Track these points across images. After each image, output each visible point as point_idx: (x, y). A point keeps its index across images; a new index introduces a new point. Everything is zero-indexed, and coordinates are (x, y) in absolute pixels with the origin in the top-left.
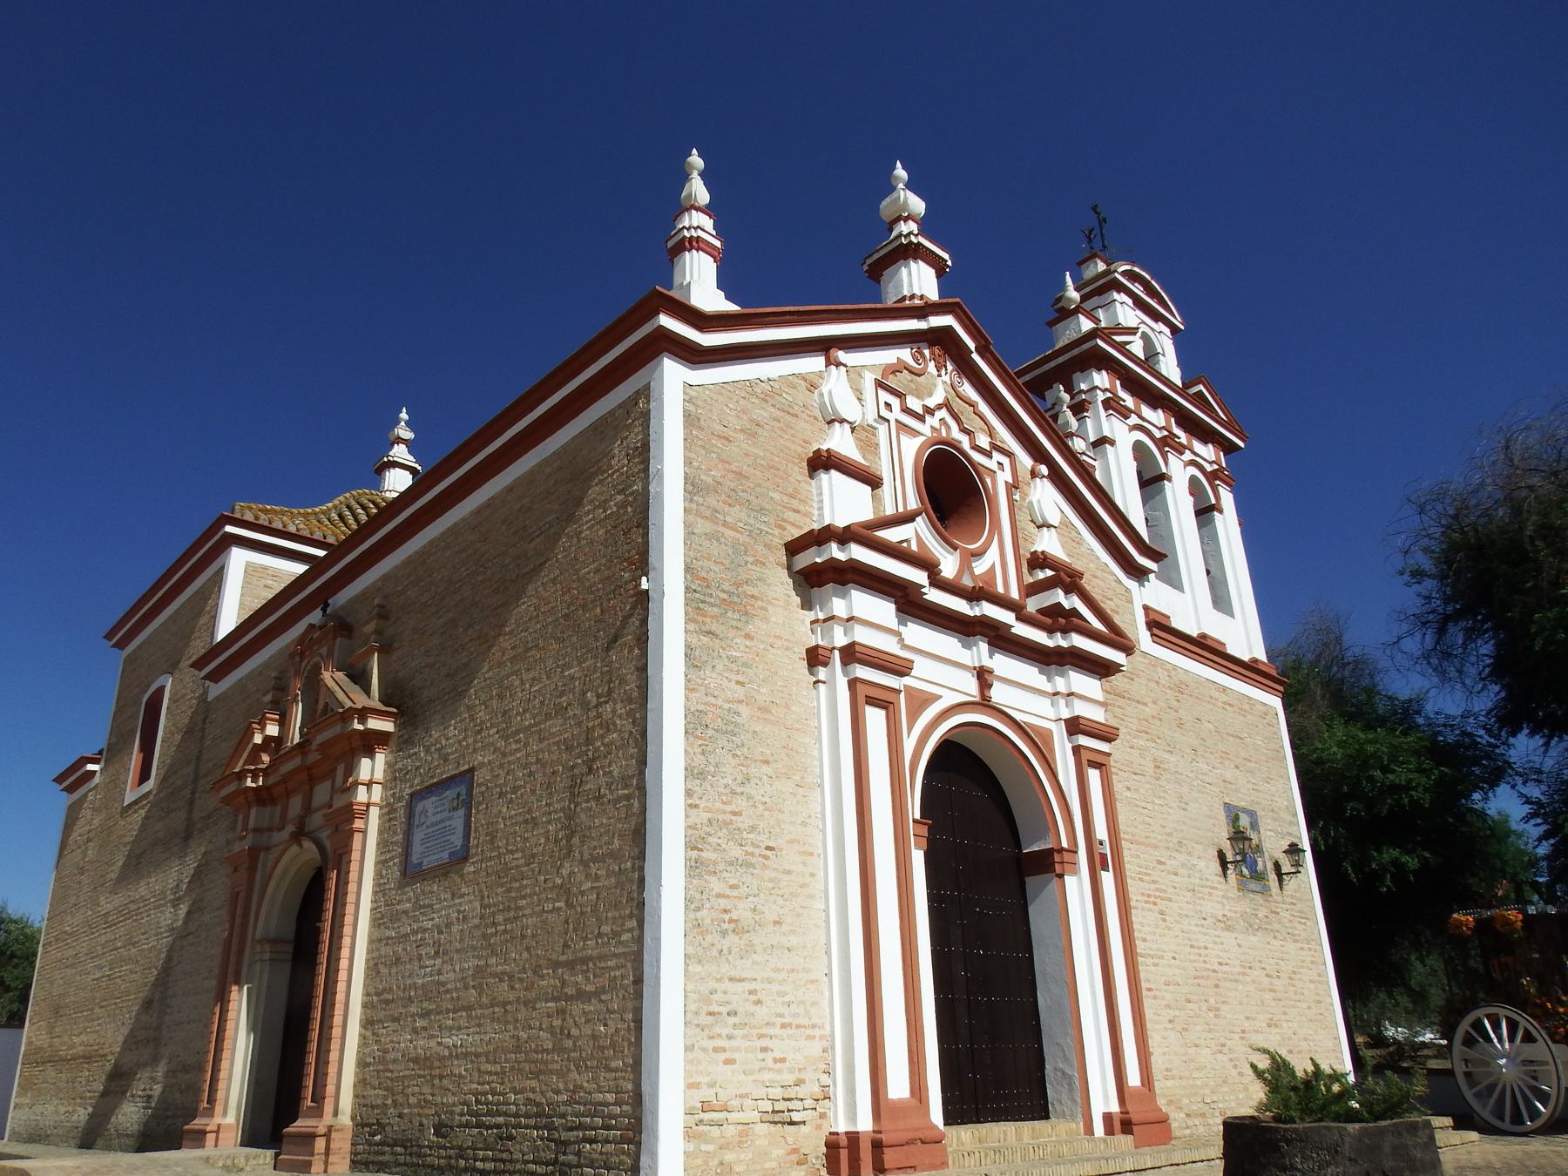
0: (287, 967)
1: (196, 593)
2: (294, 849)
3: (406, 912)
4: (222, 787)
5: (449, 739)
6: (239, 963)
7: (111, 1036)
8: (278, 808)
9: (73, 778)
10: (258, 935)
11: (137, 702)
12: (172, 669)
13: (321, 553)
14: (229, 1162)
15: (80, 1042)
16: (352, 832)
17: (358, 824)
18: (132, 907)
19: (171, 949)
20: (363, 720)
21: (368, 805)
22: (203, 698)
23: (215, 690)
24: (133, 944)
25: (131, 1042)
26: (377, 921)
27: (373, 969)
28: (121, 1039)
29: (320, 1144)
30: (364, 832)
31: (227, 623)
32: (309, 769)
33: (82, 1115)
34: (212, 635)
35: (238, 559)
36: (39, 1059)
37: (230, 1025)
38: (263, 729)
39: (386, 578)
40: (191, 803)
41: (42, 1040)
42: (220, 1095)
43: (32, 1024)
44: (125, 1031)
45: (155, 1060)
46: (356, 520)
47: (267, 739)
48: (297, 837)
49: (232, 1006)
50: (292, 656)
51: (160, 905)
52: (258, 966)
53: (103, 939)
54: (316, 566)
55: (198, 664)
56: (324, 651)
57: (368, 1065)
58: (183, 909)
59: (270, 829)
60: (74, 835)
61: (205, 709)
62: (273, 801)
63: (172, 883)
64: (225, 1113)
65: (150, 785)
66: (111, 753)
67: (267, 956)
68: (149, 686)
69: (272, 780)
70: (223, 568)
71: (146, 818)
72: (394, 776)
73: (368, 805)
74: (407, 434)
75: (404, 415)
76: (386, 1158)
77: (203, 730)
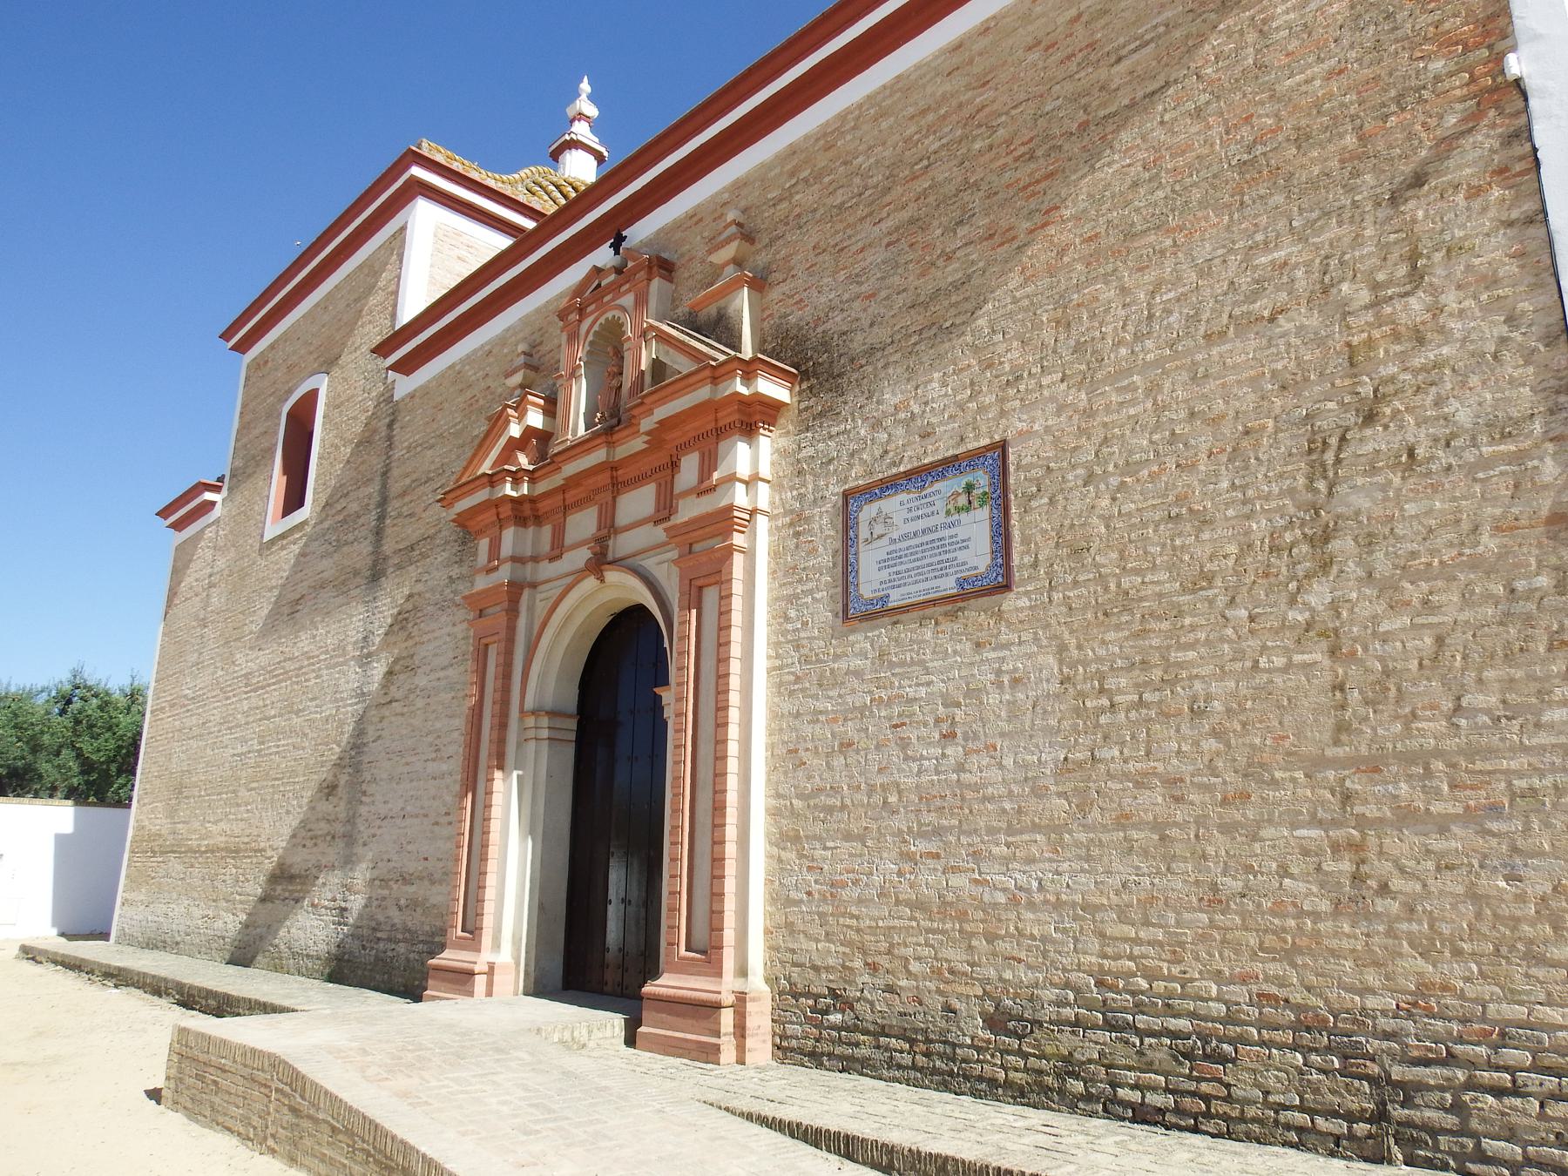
0: (570, 751)
1: (360, 267)
2: (590, 583)
3: (858, 674)
4: (457, 499)
5: (926, 405)
6: (501, 742)
7: (274, 829)
8: (547, 531)
9: (185, 510)
10: (529, 703)
11: (273, 414)
12: (328, 364)
13: (530, 224)
14: (567, 1036)
15: (219, 832)
16: (729, 551)
17: (738, 539)
18: (289, 666)
19: (361, 720)
20: (748, 377)
21: (753, 512)
22: (387, 398)
23: (405, 385)
24: (297, 713)
25: (304, 835)
26: (786, 686)
27: (789, 757)
28: (287, 832)
29: (727, 1019)
30: (750, 554)
31: (414, 301)
32: (614, 468)
33: (230, 923)
34: (394, 316)
35: (424, 216)
36: (153, 847)
37: (495, 826)
38: (521, 418)
39: (739, 186)
40: (379, 533)
41: (160, 824)
42: (488, 922)
43: (142, 805)
44: (293, 821)
45: (348, 861)
46: (565, 197)
47: (529, 432)
48: (600, 562)
49: (497, 799)
50: (562, 315)
51: (338, 664)
52: (532, 745)
53: (245, 705)
54: (524, 242)
55: (383, 349)
56: (628, 300)
57: (790, 902)
58: (379, 669)
59: (535, 559)
60: (189, 580)
61: (390, 412)
62: (538, 520)
63: (355, 636)
64: (496, 946)
65: (304, 513)
66: (243, 473)
67: (545, 733)
68: (290, 392)
69: (542, 487)
70: (403, 229)
71: (303, 554)
72: (797, 469)
73: (753, 512)
74: (591, 111)
75: (585, 86)
76: (864, 1052)
77: (390, 438)
